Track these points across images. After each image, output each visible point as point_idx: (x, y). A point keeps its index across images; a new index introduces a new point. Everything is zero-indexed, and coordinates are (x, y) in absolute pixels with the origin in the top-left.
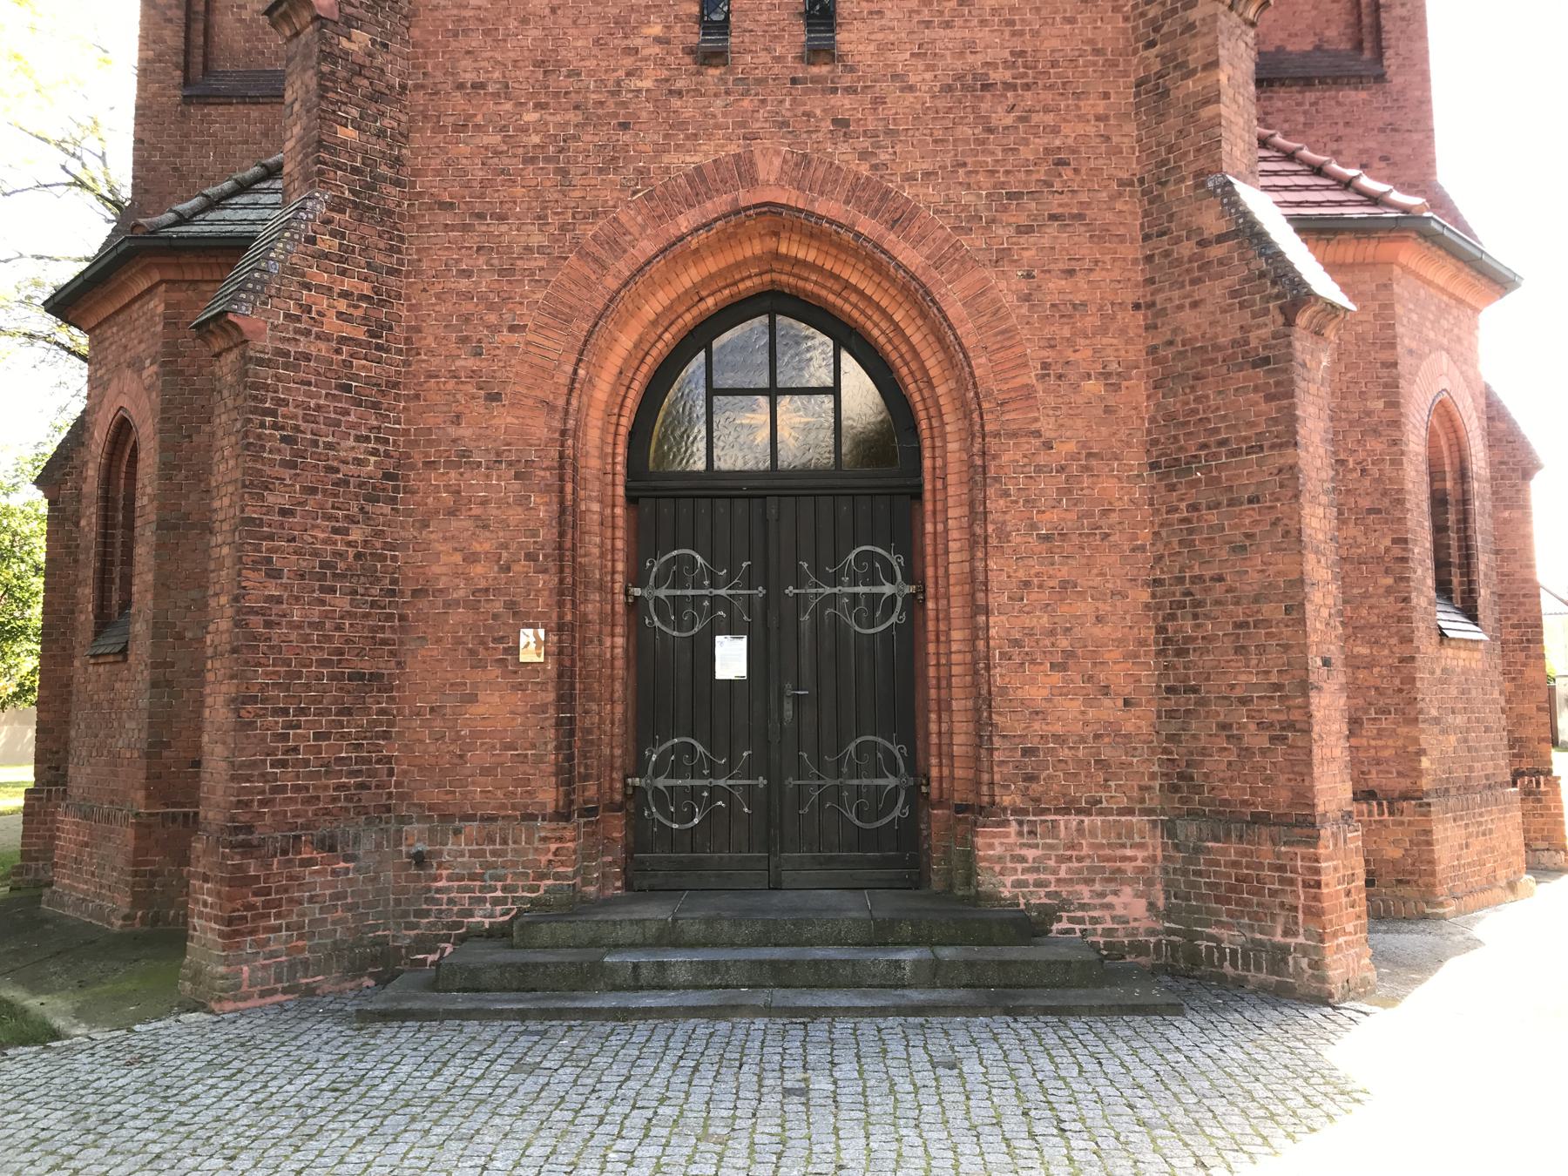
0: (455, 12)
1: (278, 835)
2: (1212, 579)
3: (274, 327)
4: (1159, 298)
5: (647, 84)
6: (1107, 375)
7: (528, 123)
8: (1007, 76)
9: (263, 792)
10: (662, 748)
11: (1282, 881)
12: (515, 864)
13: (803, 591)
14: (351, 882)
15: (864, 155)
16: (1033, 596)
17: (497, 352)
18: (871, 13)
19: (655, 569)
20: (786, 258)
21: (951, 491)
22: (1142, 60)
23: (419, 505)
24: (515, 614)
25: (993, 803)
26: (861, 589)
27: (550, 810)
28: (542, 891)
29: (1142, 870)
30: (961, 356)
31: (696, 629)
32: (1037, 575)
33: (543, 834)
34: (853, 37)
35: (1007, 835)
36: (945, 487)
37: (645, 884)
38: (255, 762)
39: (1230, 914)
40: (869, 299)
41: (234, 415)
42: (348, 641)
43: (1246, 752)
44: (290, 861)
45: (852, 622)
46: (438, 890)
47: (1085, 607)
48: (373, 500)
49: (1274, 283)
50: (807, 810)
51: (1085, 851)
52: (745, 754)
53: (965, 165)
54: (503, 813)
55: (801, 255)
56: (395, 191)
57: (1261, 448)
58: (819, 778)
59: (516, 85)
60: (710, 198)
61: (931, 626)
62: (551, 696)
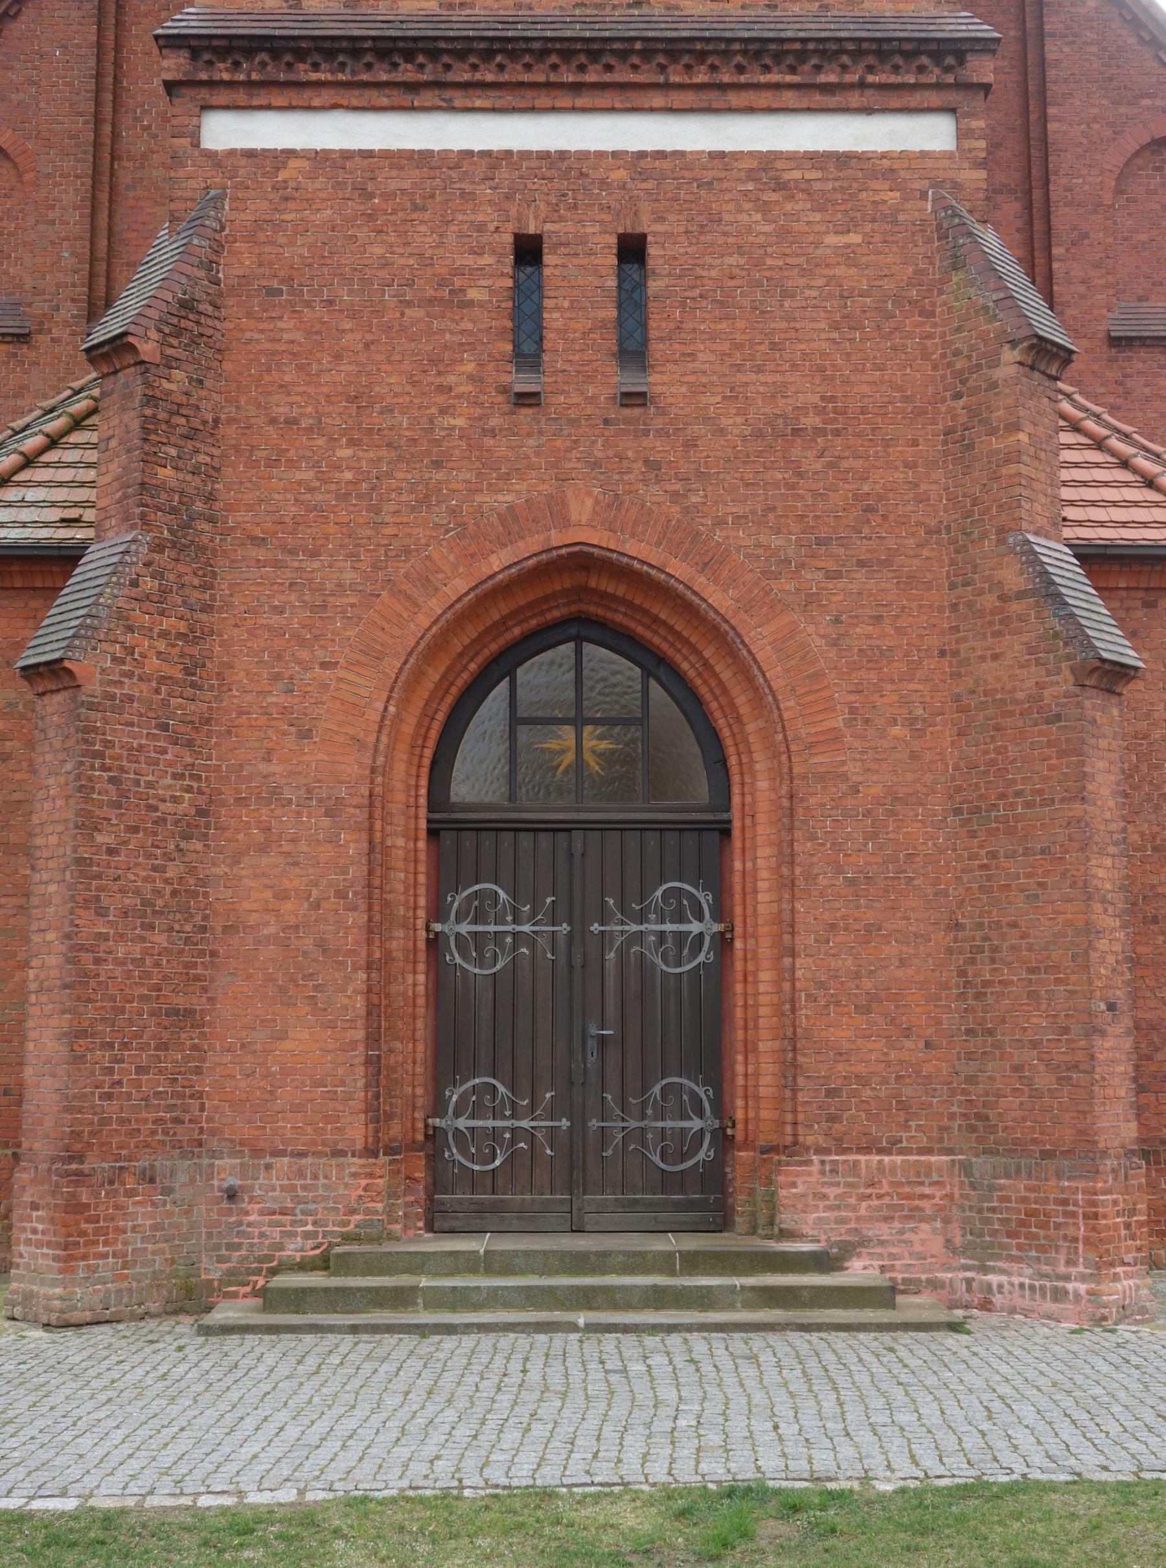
0: (268, 346)
1: (105, 1165)
2: (1008, 924)
3: (103, 670)
4: (963, 647)
5: (460, 422)
6: (912, 721)
7: (341, 459)
8: (817, 421)
9: (92, 1123)
10: (463, 1089)
11: (1067, 1214)
12: (325, 1199)
13: (608, 928)
14: (170, 1214)
15: (675, 496)
16: (839, 939)
17: (309, 689)
18: (684, 355)
19: (456, 904)
20: (595, 592)
21: (761, 830)
22: (950, 410)
23: (230, 841)
24: (324, 951)
25: (795, 1143)
26: (669, 927)
27: (359, 1146)
28: (352, 1226)
29: (941, 1209)
30: (770, 698)
31: (498, 967)
32: (843, 918)
33: (353, 1170)
34: (665, 378)
35: (810, 1174)
36: (754, 825)
37: (446, 1226)
38: (85, 1095)
39: (1020, 1247)
40: (678, 635)
41: (62, 756)
42: (165, 977)
43: (1036, 1095)
44: (116, 1191)
45: (658, 961)
46: (249, 1225)
47: (891, 950)
48: (187, 837)
49: (1066, 644)
50: (610, 1152)
51: (886, 1188)
52: (548, 1095)
53: (774, 509)
54: (313, 1149)
55: (610, 590)
56: (207, 527)
57: (1053, 800)
58: (623, 1120)
59: (329, 421)
60: (523, 538)
61: (739, 966)
62: (360, 1034)
